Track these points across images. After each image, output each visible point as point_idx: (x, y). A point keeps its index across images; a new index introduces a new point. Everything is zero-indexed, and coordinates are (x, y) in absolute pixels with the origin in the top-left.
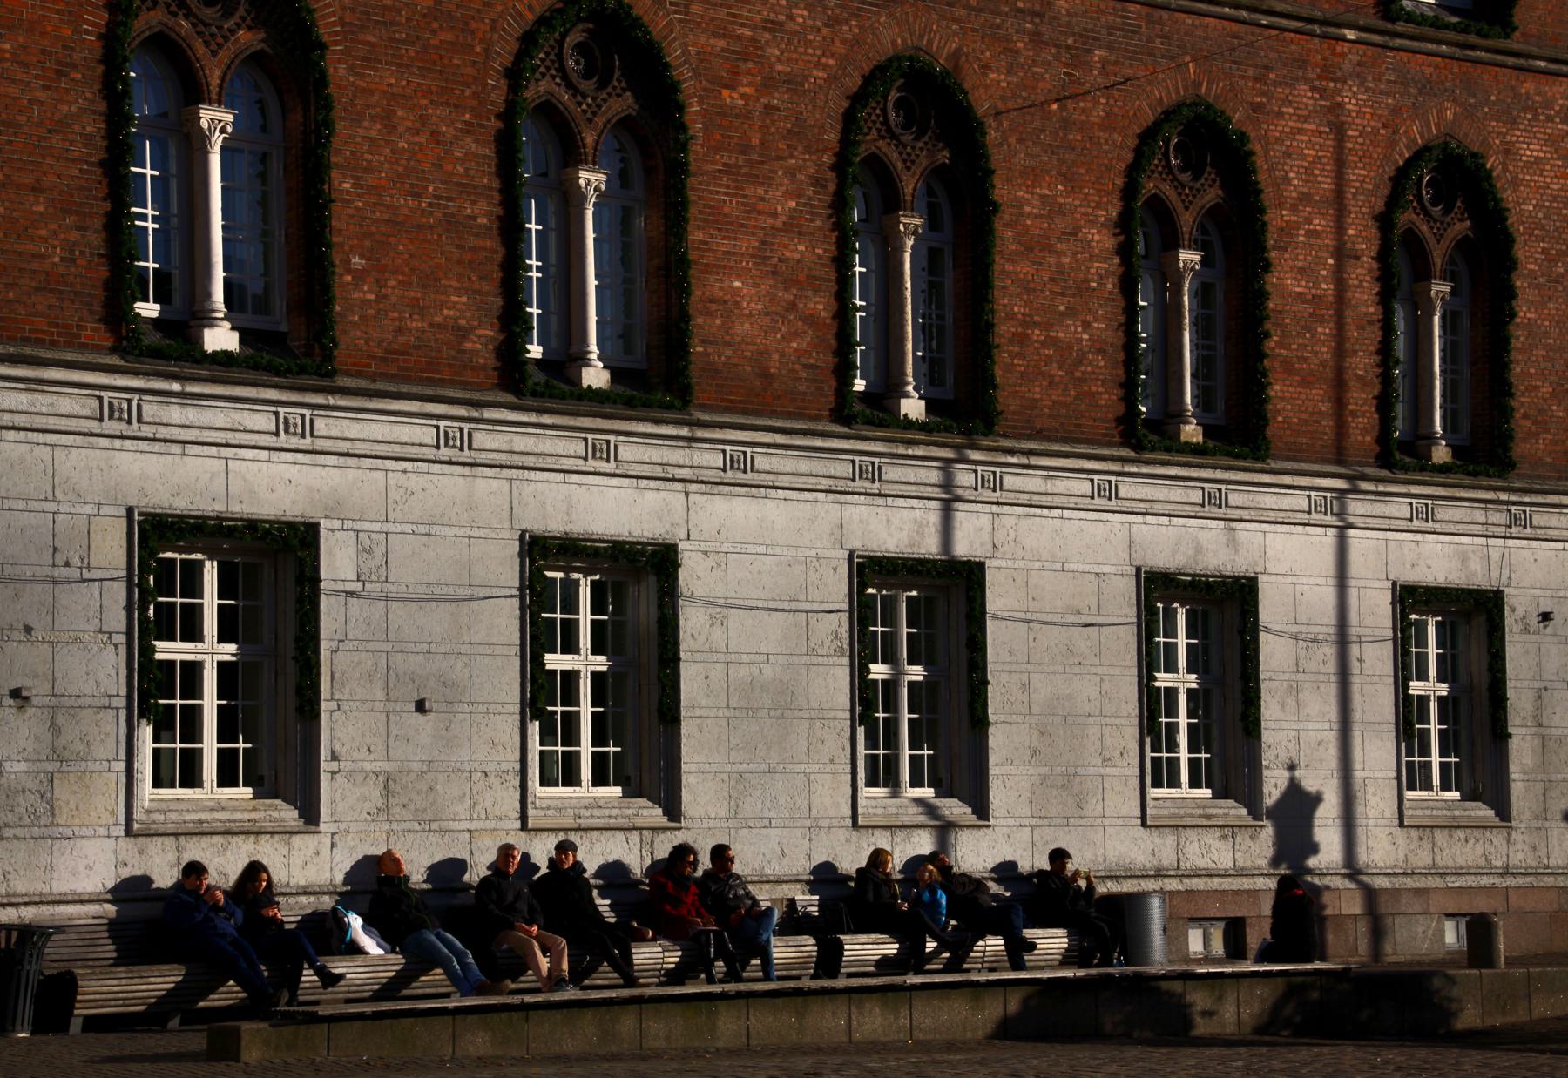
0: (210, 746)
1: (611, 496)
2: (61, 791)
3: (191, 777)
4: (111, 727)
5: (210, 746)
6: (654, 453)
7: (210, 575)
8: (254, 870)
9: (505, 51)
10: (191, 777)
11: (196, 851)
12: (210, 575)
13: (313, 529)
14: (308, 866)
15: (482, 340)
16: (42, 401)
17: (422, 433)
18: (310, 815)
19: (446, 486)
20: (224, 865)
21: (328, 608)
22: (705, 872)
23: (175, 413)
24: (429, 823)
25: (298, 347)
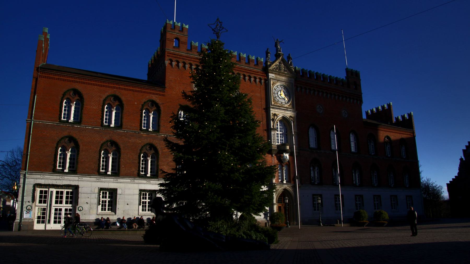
0: (147, 208)
1: (110, 183)
2: (91, 211)
3: (105, 210)
4: (96, 206)
5: (147, 208)
6: (154, 182)
7: (108, 193)
8: (108, 218)
9: (140, 148)
10: (105, 210)
11: (108, 216)
12: (108, 193)
13: (117, 189)
14: (113, 218)
15: (136, 173)
16: (91, 179)
17: (129, 180)
18: (116, 213)
19: (132, 185)
20: (105, 217)
21: (118, 196)
22: (254, 217)
23: (104, 179)
24: (128, 214)
25: (116, 173)
